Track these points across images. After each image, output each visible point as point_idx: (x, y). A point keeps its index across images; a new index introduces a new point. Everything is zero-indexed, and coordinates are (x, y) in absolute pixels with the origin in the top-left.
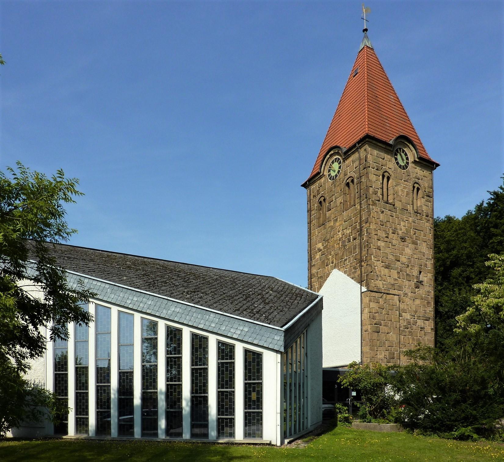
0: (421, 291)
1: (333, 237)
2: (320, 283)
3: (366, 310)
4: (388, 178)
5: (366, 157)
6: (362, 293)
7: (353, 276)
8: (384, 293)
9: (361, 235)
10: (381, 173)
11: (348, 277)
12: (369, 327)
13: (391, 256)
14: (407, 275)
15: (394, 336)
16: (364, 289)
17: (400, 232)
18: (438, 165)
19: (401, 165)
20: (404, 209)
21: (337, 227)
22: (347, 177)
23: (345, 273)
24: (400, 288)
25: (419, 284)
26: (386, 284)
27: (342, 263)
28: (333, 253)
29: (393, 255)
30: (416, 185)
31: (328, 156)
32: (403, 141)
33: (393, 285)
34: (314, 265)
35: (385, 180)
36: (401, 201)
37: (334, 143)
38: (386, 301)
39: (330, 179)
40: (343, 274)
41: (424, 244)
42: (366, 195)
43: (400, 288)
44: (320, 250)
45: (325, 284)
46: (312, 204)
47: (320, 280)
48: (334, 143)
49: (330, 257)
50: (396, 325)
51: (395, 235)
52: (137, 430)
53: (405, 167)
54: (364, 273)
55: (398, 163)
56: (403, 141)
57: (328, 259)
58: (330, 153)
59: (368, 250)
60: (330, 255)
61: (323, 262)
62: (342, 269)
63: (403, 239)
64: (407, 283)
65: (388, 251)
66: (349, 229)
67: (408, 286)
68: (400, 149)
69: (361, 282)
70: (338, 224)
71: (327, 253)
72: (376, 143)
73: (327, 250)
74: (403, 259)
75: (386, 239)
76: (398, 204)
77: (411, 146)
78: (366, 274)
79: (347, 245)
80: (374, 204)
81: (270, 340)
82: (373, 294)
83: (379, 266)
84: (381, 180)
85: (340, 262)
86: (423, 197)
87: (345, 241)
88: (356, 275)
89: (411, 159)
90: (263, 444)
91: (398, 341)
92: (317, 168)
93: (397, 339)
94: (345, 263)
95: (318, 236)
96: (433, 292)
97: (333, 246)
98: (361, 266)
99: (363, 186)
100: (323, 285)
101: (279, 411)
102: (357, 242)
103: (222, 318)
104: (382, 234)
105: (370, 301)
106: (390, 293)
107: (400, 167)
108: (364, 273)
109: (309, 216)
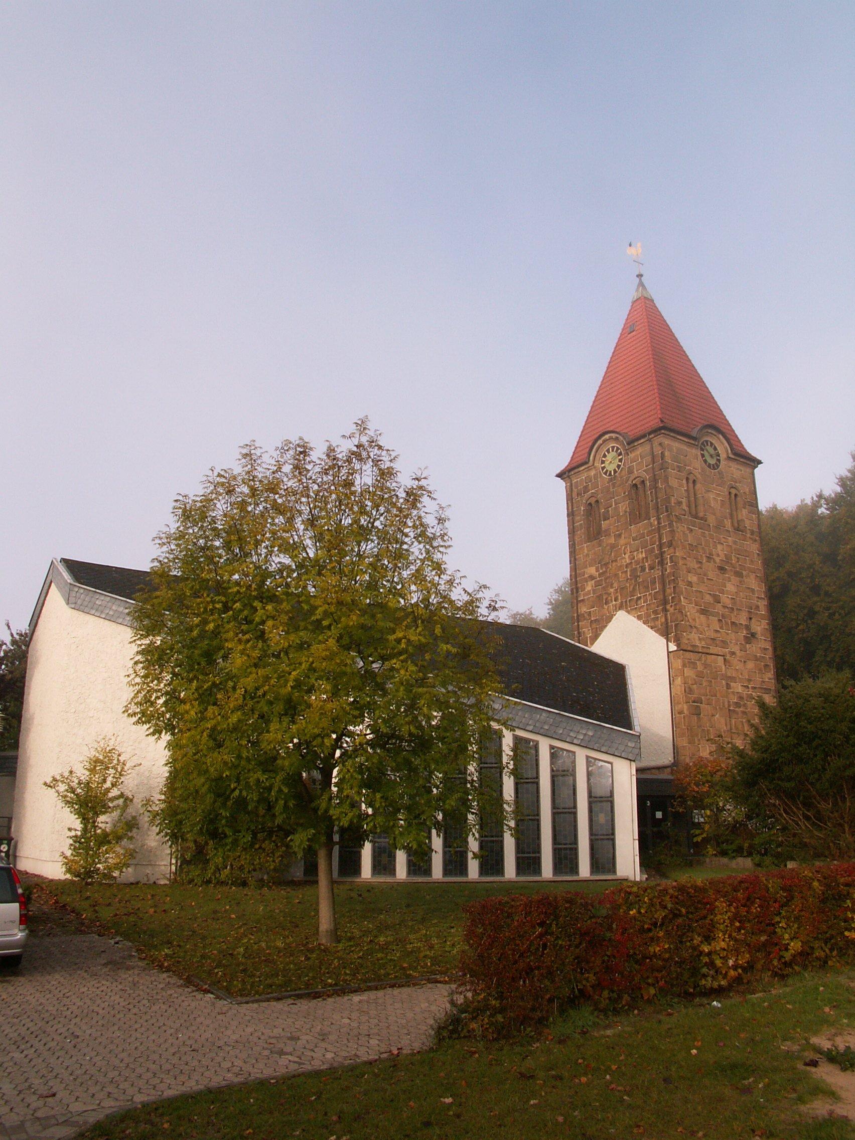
0: (754, 648)
1: (616, 561)
2: (594, 630)
3: (679, 681)
4: (694, 482)
5: (663, 454)
6: (669, 652)
7: (653, 624)
8: (703, 653)
9: (662, 563)
10: (684, 474)
11: (645, 626)
12: (685, 707)
13: (708, 596)
14: (733, 623)
15: (723, 720)
16: (673, 647)
17: (717, 559)
18: (760, 462)
19: (710, 464)
20: (719, 526)
21: (622, 546)
22: (633, 477)
23: (639, 618)
24: (724, 644)
25: (751, 637)
26: (703, 639)
27: (633, 603)
28: (615, 585)
29: (710, 594)
30: (733, 491)
31: (600, 442)
32: (710, 431)
33: (713, 639)
34: (583, 600)
35: (691, 485)
36: (714, 514)
37: (610, 424)
38: (706, 666)
39: (605, 473)
40: (635, 619)
41: (753, 576)
42: (666, 507)
43: (724, 644)
44: (592, 577)
45: (603, 634)
46: (575, 505)
47: (594, 626)
48: (610, 424)
49: (612, 590)
50: (723, 703)
51: (711, 565)
52: (437, 871)
53: (715, 467)
54: (671, 622)
55: (705, 461)
56: (710, 431)
57: (609, 594)
58: (603, 438)
59: (674, 587)
60: (612, 587)
61: (600, 597)
62: (634, 612)
63: (722, 569)
64: (733, 636)
65: (702, 588)
66: (642, 552)
67: (735, 639)
68: (707, 441)
69: (665, 632)
70: (622, 541)
71: (606, 583)
72: (675, 435)
73: (606, 579)
74: (725, 599)
75: (699, 571)
76: (711, 520)
77: (721, 437)
78: (673, 624)
79: (639, 576)
80: (679, 519)
81: (622, 748)
82: (688, 655)
83: (691, 610)
84: (685, 485)
85: (630, 600)
86: (744, 508)
87: (636, 569)
88: (658, 623)
89: (723, 456)
90: (618, 880)
91: (729, 727)
92: (583, 452)
93: (726, 725)
94: (639, 602)
95: (587, 555)
96: (770, 648)
97: (616, 575)
98: (665, 610)
99: (661, 495)
100: (600, 634)
101: (636, 837)
102: (657, 573)
103: (558, 719)
104: (693, 564)
105: (684, 665)
106: (711, 652)
107: (709, 466)
108: (671, 622)
109: (571, 523)
